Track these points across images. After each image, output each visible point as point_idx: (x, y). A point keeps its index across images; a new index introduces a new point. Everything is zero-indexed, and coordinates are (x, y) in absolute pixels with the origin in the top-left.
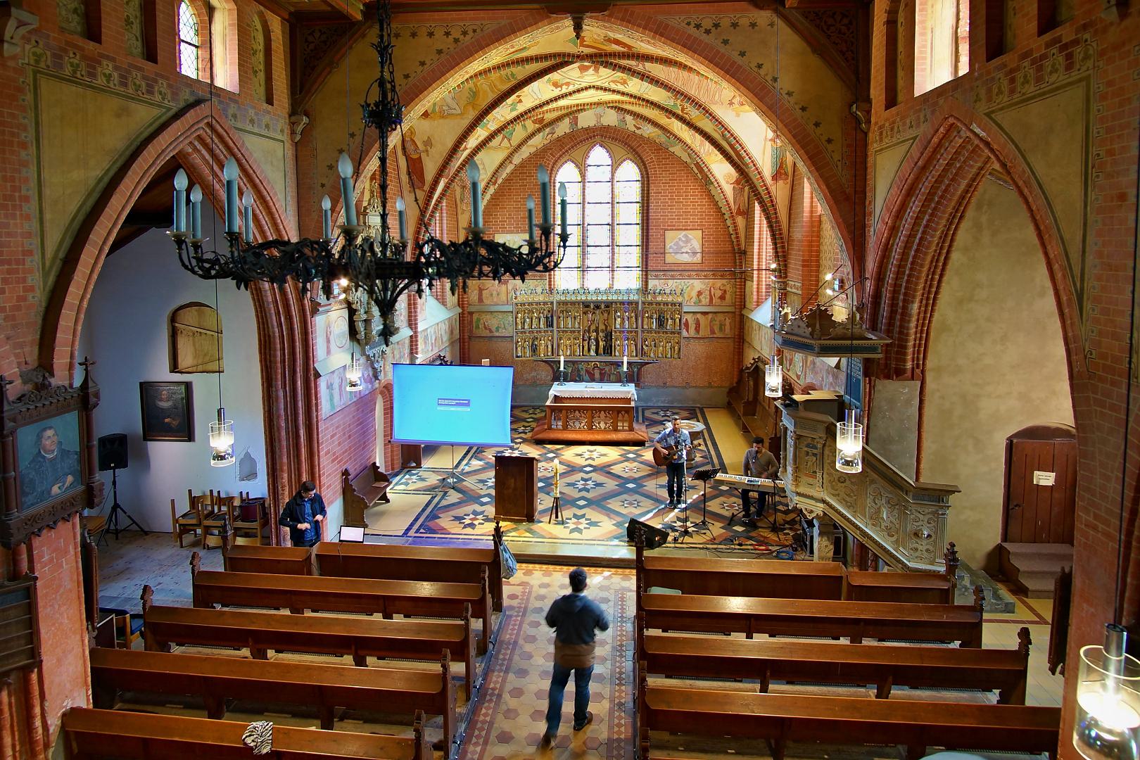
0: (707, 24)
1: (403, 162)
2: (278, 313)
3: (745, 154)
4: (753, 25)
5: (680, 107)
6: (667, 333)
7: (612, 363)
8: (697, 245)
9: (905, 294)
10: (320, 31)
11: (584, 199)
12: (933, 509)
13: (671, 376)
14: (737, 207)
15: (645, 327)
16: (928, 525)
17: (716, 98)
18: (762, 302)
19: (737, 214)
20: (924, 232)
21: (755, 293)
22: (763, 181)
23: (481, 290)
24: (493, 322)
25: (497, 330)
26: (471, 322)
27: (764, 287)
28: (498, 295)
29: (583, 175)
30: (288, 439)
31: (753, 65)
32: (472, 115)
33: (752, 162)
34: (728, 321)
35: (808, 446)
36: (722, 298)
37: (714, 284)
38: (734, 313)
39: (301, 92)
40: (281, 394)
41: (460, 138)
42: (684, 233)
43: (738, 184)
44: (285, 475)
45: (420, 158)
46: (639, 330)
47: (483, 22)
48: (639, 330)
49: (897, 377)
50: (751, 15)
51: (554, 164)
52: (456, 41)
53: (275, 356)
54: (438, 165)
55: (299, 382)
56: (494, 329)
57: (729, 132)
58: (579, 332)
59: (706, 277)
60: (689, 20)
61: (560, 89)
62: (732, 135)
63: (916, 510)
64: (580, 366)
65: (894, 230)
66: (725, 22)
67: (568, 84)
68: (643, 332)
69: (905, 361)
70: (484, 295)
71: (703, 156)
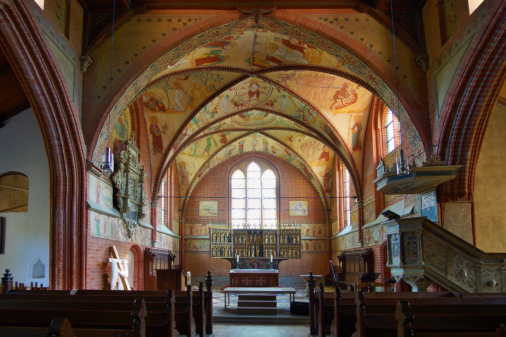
0: (331, 18)
1: (151, 138)
2: (63, 162)
3: (338, 136)
4: (357, 20)
5: (302, 117)
6: (293, 245)
7: (264, 260)
8: (305, 207)
9: (463, 147)
10: (102, 15)
11: (246, 186)
12: (498, 267)
13: (294, 271)
14: (326, 188)
15: (281, 242)
16: (495, 278)
17: (323, 105)
18: (343, 229)
19: (326, 191)
20: (477, 101)
21: (339, 225)
22: (348, 150)
23: (191, 229)
24: (198, 244)
25: (200, 248)
26: (186, 244)
27: (343, 222)
28: (201, 231)
29: (246, 175)
30: (65, 241)
31: (359, 39)
32: (190, 111)
33: (342, 140)
34: (323, 244)
35: (409, 238)
36: (320, 232)
37: (315, 226)
38: (326, 240)
39: (89, 44)
40: (62, 212)
41: (182, 126)
42: (299, 202)
43: (326, 177)
44: (61, 263)
45: (160, 135)
46: (278, 244)
47: (201, 15)
48: (278, 244)
49: (459, 198)
50: (355, 15)
51: (231, 169)
52: (185, 24)
53: (60, 188)
54: (170, 139)
55: (75, 207)
56: (198, 248)
57: (330, 124)
58: (245, 245)
59: (311, 223)
60: (321, 17)
61: (237, 107)
62: (332, 126)
63: (487, 269)
64: (246, 261)
65: (455, 106)
66: (341, 18)
67: (242, 105)
68: (280, 245)
69: (464, 188)
70: (193, 231)
71: (308, 163)
